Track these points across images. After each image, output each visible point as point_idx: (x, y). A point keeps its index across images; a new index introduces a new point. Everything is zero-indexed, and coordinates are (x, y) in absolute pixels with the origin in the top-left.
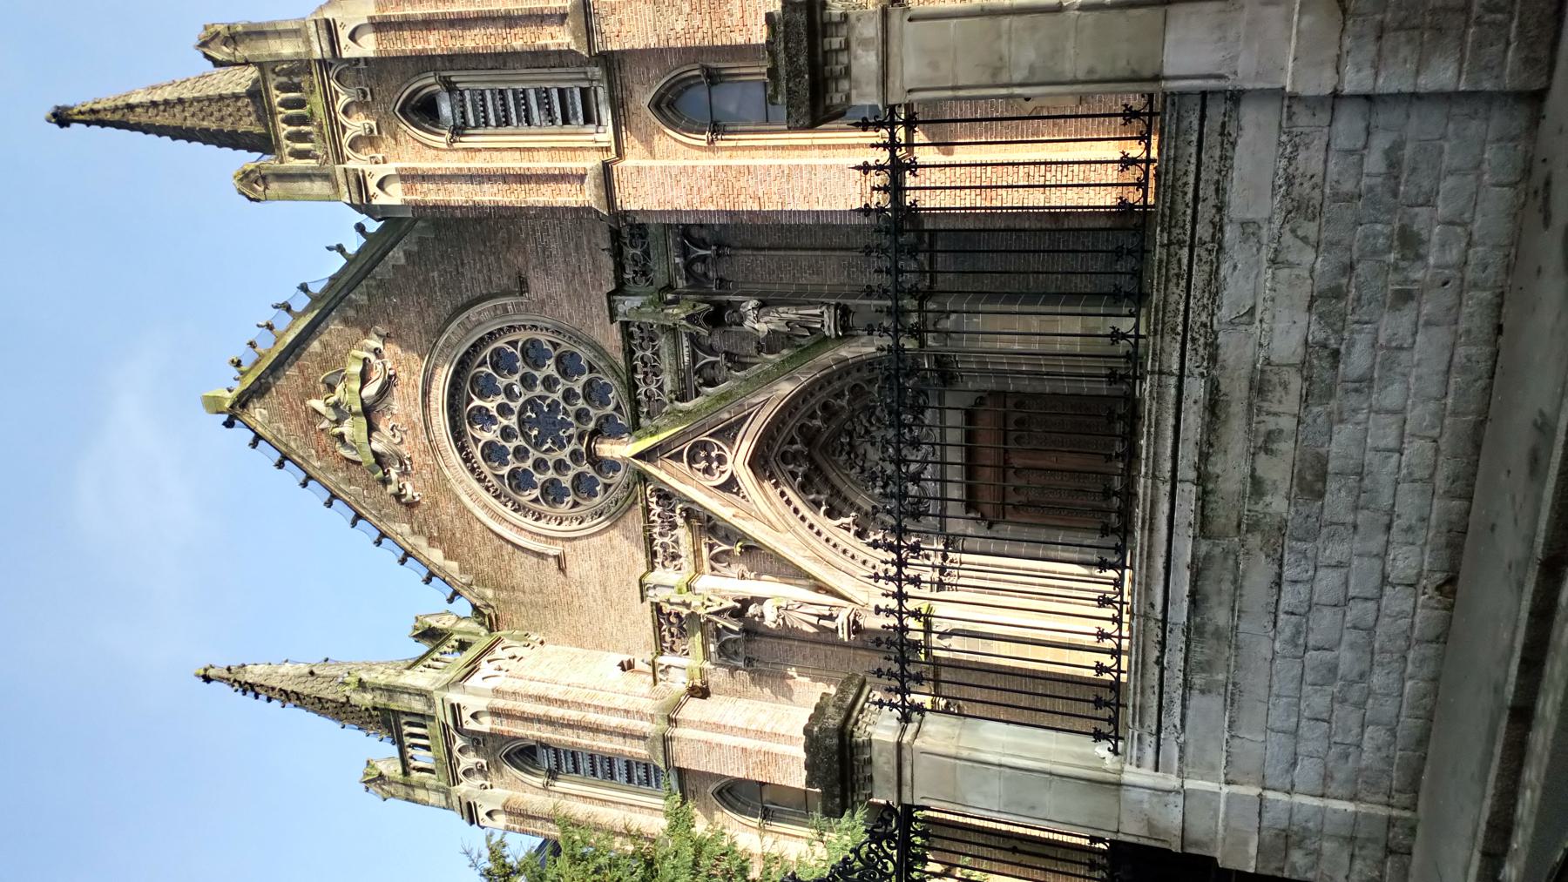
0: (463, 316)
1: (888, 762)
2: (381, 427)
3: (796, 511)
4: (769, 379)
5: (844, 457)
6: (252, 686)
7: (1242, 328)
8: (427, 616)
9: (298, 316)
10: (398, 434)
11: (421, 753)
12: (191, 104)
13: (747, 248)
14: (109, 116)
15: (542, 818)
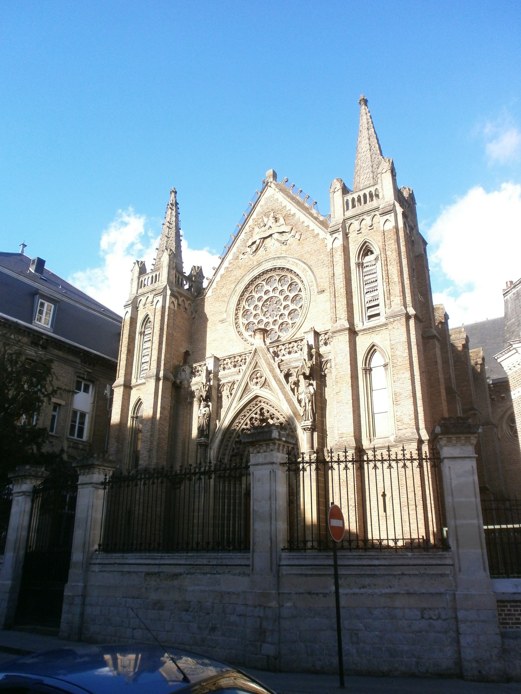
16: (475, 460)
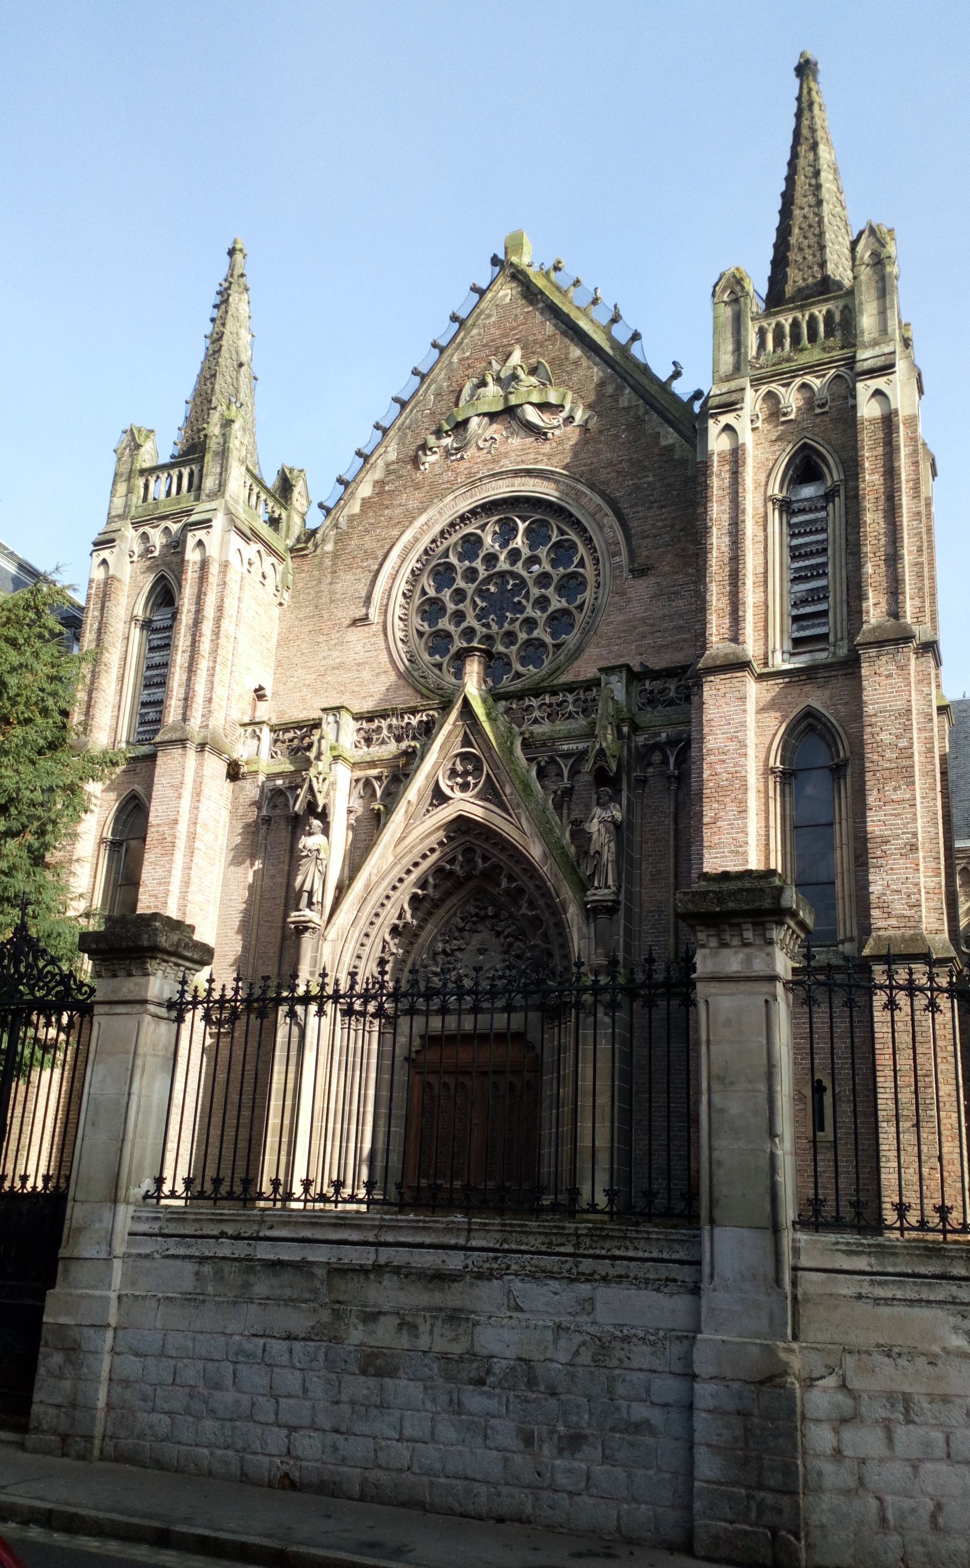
0: (607, 510)
1: (130, 992)
2: (495, 426)
3: (416, 864)
4: (545, 834)
5: (473, 911)
6: (226, 301)
7: (505, 1301)
8: (305, 481)
9: (607, 331)
10: (487, 444)
11: (163, 488)
12: (816, 214)
13: (676, 807)
14: (806, 123)
15: (102, 616)
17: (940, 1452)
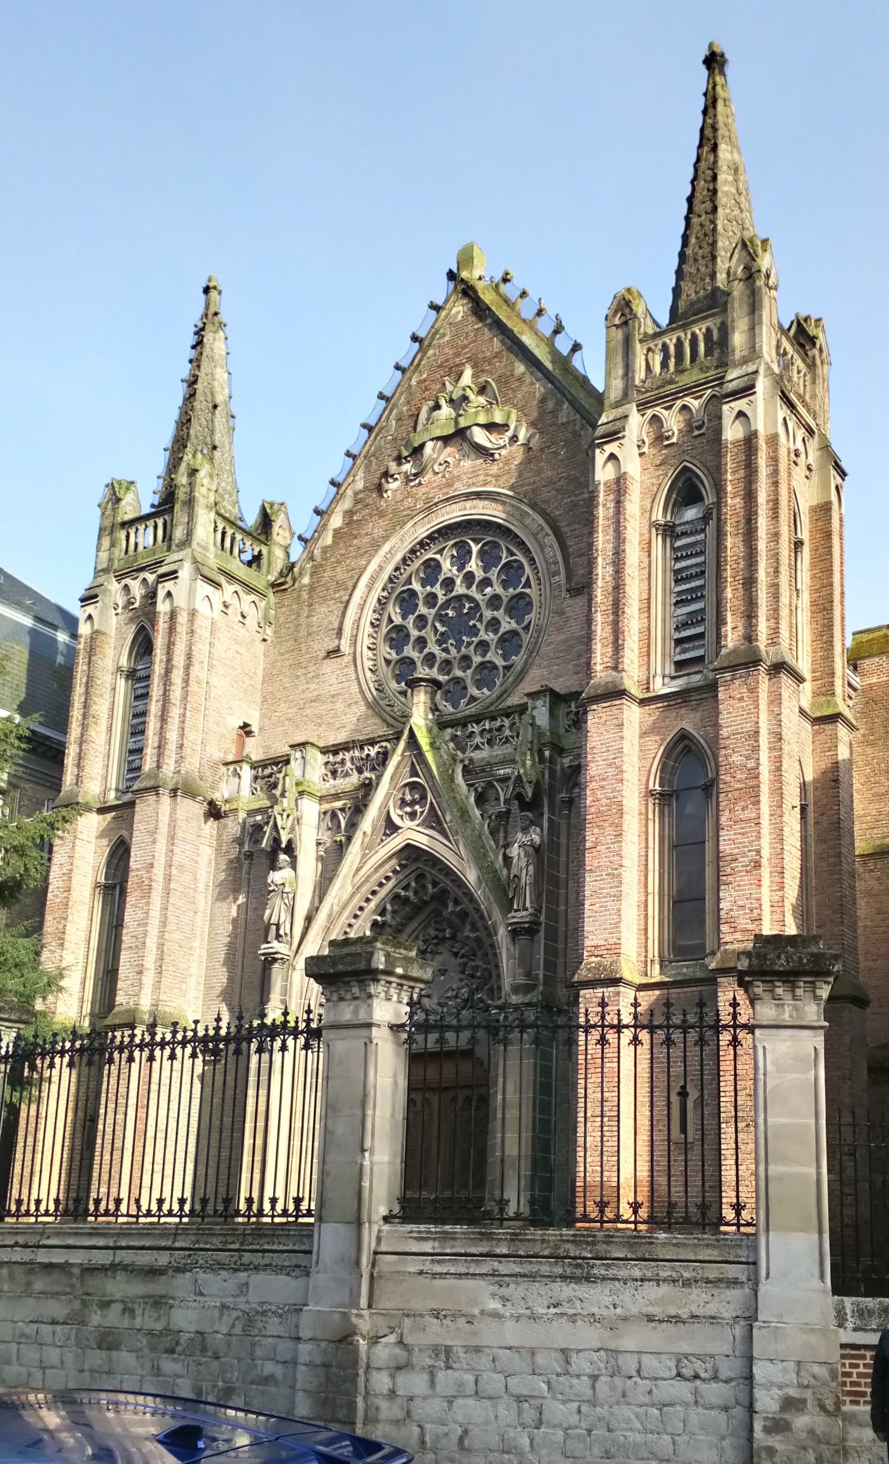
0: (548, 530)
2: (449, 449)
4: (480, 857)
5: (433, 933)
8: (286, 514)
9: (550, 342)
10: (442, 468)
16: (822, 1032)
17: (470, 1389)
